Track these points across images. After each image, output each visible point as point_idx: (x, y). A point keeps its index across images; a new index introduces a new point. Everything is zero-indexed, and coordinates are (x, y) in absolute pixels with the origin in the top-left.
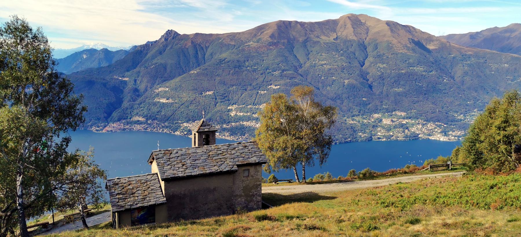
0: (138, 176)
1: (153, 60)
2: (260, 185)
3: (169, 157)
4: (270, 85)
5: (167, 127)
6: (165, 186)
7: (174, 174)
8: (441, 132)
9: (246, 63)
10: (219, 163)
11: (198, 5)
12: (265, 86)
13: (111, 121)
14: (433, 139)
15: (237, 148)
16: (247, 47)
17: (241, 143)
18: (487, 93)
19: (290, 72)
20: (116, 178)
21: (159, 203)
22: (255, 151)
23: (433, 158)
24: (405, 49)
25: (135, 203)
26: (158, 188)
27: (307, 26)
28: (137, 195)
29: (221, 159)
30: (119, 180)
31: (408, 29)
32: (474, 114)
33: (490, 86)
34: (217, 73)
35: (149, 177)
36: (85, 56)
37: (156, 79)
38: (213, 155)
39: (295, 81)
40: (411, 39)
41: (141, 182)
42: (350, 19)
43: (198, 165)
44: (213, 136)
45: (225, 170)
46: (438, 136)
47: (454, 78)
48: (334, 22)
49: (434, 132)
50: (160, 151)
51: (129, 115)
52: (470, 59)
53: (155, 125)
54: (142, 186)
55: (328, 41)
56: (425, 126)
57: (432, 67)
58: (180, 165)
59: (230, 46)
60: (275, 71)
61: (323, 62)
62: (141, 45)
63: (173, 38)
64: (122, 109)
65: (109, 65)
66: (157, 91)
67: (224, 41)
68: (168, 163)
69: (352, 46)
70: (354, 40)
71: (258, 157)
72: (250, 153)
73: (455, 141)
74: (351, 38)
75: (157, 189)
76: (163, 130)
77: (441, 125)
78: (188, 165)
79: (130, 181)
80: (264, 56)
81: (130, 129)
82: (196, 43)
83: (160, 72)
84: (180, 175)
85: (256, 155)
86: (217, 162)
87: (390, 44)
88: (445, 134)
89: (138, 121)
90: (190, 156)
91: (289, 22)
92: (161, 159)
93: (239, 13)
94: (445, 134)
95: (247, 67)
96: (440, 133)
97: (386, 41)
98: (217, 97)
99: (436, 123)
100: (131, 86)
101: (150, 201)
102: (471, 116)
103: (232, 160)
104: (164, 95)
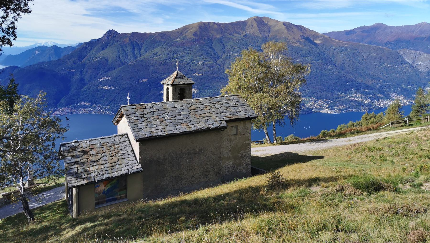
0: (103, 138)
1: (97, 55)
2: (249, 144)
3: (142, 113)
4: (195, 73)
5: (109, 110)
6: (140, 148)
7: (152, 133)
8: (329, 107)
9: (174, 56)
10: (205, 119)
11: (135, 11)
12: (190, 74)
13: (59, 106)
14: (323, 112)
15: (222, 102)
16: (175, 43)
17: (224, 97)
18: (361, 76)
19: (210, 62)
20: (74, 141)
21: (133, 171)
22: (242, 105)
23: (344, 124)
24: (298, 43)
25: (101, 173)
26: (130, 153)
27: (222, 26)
28: (103, 162)
29: (205, 114)
30: (77, 144)
31: (300, 28)
32: (352, 92)
33: (363, 70)
34: (151, 64)
35: (117, 139)
36: (37, 52)
37: (100, 70)
38: (195, 109)
39: (215, 69)
40: (303, 36)
41: (108, 146)
42: (256, 21)
43: (180, 121)
44: (189, 91)
45: (213, 127)
46: (327, 110)
47: (336, 65)
48: (244, 23)
49: (323, 107)
50: (130, 106)
51: (76, 100)
52: (347, 50)
53: (99, 108)
54: (109, 150)
55: (239, 38)
56: (317, 102)
57: (319, 57)
58: (158, 122)
59: (161, 42)
60: (198, 62)
61: (236, 54)
62: (86, 42)
63: (114, 36)
64: (70, 96)
65: (58, 59)
66: (100, 80)
67: (156, 38)
68: (142, 120)
69: (258, 41)
70: (259, 36)
71: (246, 111)
72: (237, 107)
73: (339, 113)
74: (257, 35)
75: (128, 153)
76: (106, 113)
77: (328, 101)
78: (167, 121)
79: (92, 145)
80: (189, 50)
81: (77, 113)
82: (133, 40)
83: (102, 64)
84: (160, 134)
85: (243, 109)
86: (202, 118)
87: (287, 39)
88: (332, 108)
89: (84, 105)
90: (168, 111)
91: (208, 23)
92: (134, 115)
93: (168, 17)
94: (332, 108)
95: (175, 59)
96: (328, 107)
97: (284, 37)
98: (151, 84)
99: (325, 100)
100: (77, 76)
101: (120, 169)
102: (350, 94)
103: (219, 115)
104: (107, 83)
